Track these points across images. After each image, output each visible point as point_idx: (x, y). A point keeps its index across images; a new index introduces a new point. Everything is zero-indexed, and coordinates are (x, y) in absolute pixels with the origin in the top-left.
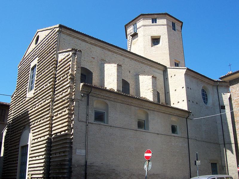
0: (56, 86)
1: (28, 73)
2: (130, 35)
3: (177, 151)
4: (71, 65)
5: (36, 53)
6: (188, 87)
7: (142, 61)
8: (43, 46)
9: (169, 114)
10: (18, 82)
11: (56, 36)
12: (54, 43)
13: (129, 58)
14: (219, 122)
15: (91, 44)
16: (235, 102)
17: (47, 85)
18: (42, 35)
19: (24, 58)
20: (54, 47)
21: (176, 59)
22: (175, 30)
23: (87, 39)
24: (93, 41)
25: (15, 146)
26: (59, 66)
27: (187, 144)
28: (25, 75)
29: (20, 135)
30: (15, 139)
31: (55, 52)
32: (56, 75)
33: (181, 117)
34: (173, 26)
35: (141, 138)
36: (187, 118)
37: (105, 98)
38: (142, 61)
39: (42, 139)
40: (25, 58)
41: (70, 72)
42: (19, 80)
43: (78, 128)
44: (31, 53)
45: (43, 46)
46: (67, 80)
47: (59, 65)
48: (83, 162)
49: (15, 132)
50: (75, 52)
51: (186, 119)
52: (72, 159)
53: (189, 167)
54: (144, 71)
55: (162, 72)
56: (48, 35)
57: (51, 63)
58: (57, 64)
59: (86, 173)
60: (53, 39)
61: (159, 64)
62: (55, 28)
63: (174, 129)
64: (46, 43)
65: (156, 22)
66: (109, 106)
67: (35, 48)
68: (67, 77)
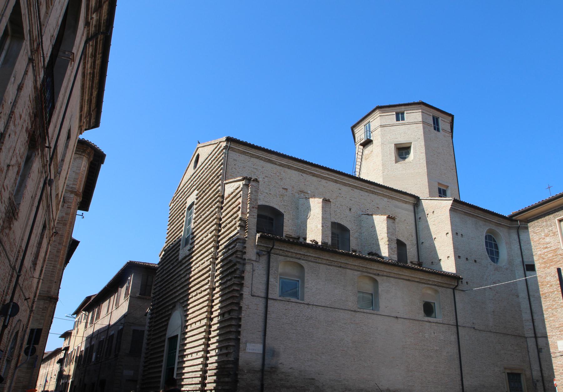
0: (220, 238)
1: (183, 216)
2: (360, 143)
3: (435, 348)
4: (241, 204)
5: (195, 183)
6: (457, 233)
7: (372, 190)
8: (204, 171)
9: (418, 282)
10: (168, 229)
11: (222, 155)
12: (219, 167)
13: (350, 186)
14: (523, 295)
15: (281, 165)
16: (538, 260)
17: (207, 236)
18: (204, 152)
19: (177, 190)
20: (219, 174)
21: (441, 182)
22: (438, 130)
23: (274, 158)
24: (284, 161)
25: (161, 337)
26: (226, 205)
27: (455, 336)
28: (178, 219)
29: (167, 318)
30: (161, 325)
31: (220, 182)
32: (221, 219)
33: (443, 287)
34: (434, 123)
35: (364, 325)
36: (454, 289)
37: (299, 256)
38: (374, 190)
39: (198, 324)
40: (180, 191)
41: (240, 216)
42: (170, 227)
43: (250, 307)
44: (188, 183)
45: (204, 171)
46: (236, 229)
47: (225, 202)
48: (257, 364)
49: (162, 314)
50: (248, 183)
51: (452, 290)
52: (238, 359)
53: (460, 379)
54: (378, 207)
55: (411, 208)
56: (211, 153)
57: (213, 201)
58: (222, 203)
59: (262, 385)
60: (217, 160)
61: (405, 194)
62: (220, 142)
63: (428, 309)
64: (208, 167)
65: (403, 119)
66: (306, 270)
67: (193, 174)
68: (235, 224)
